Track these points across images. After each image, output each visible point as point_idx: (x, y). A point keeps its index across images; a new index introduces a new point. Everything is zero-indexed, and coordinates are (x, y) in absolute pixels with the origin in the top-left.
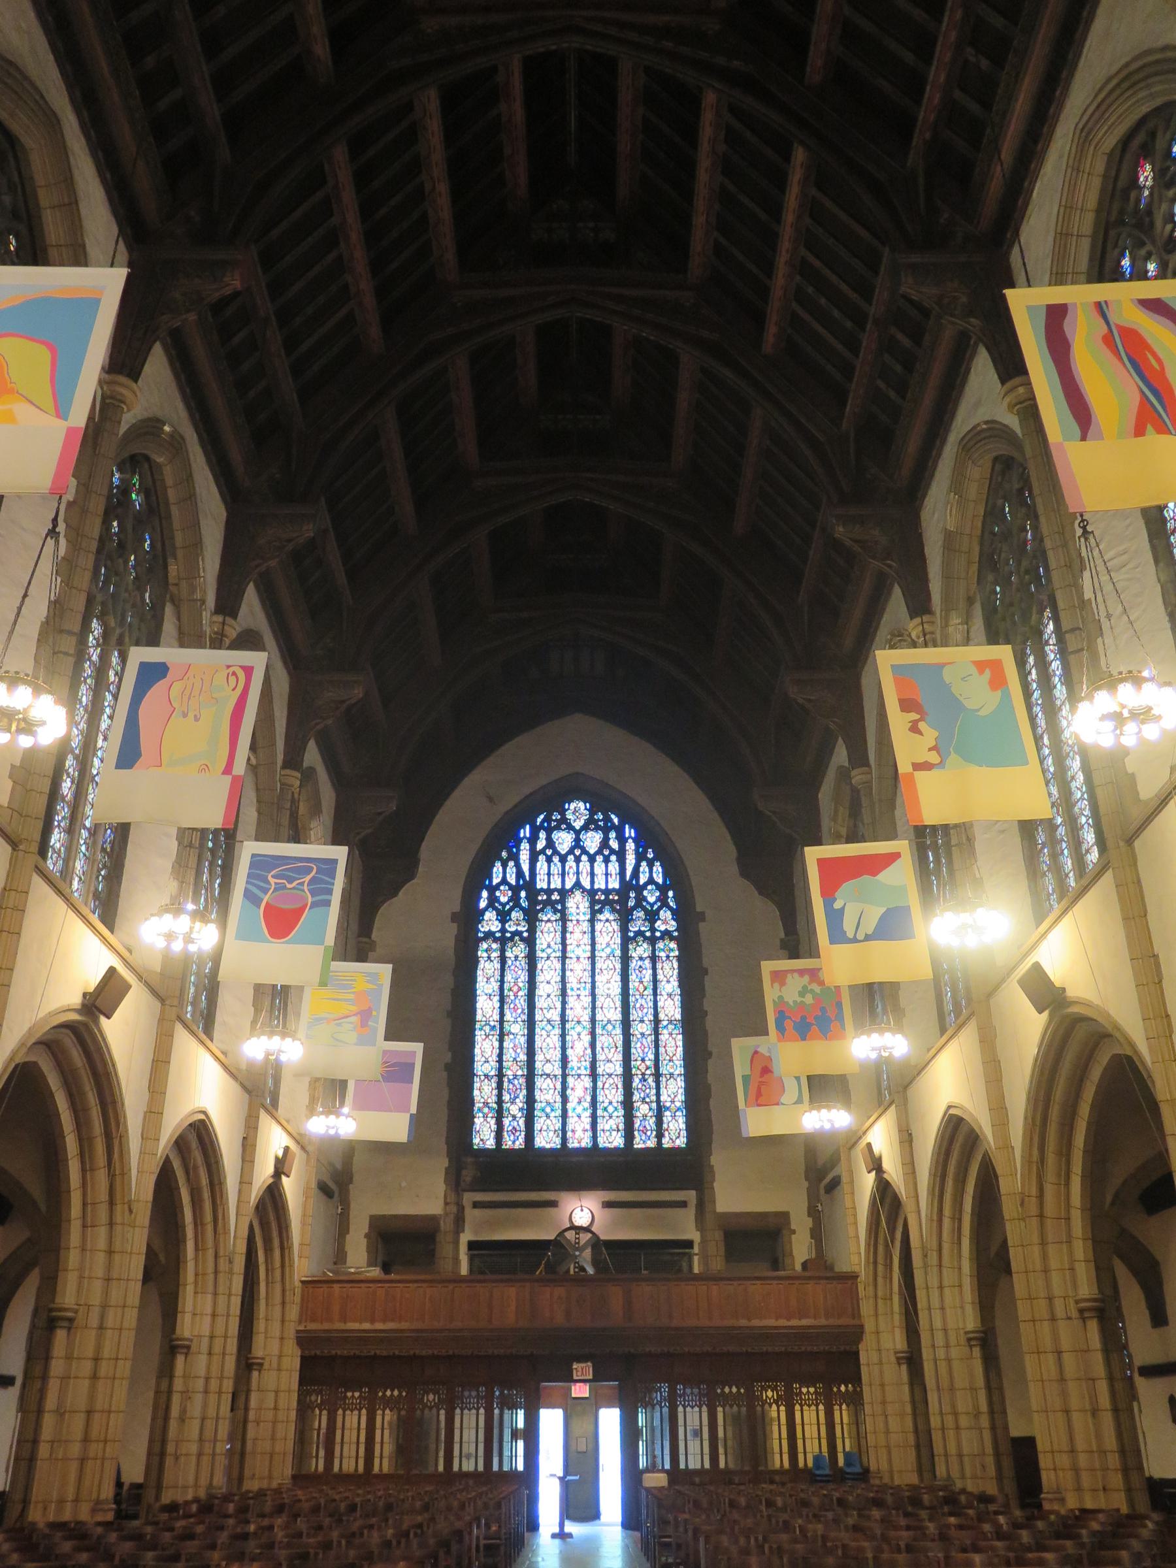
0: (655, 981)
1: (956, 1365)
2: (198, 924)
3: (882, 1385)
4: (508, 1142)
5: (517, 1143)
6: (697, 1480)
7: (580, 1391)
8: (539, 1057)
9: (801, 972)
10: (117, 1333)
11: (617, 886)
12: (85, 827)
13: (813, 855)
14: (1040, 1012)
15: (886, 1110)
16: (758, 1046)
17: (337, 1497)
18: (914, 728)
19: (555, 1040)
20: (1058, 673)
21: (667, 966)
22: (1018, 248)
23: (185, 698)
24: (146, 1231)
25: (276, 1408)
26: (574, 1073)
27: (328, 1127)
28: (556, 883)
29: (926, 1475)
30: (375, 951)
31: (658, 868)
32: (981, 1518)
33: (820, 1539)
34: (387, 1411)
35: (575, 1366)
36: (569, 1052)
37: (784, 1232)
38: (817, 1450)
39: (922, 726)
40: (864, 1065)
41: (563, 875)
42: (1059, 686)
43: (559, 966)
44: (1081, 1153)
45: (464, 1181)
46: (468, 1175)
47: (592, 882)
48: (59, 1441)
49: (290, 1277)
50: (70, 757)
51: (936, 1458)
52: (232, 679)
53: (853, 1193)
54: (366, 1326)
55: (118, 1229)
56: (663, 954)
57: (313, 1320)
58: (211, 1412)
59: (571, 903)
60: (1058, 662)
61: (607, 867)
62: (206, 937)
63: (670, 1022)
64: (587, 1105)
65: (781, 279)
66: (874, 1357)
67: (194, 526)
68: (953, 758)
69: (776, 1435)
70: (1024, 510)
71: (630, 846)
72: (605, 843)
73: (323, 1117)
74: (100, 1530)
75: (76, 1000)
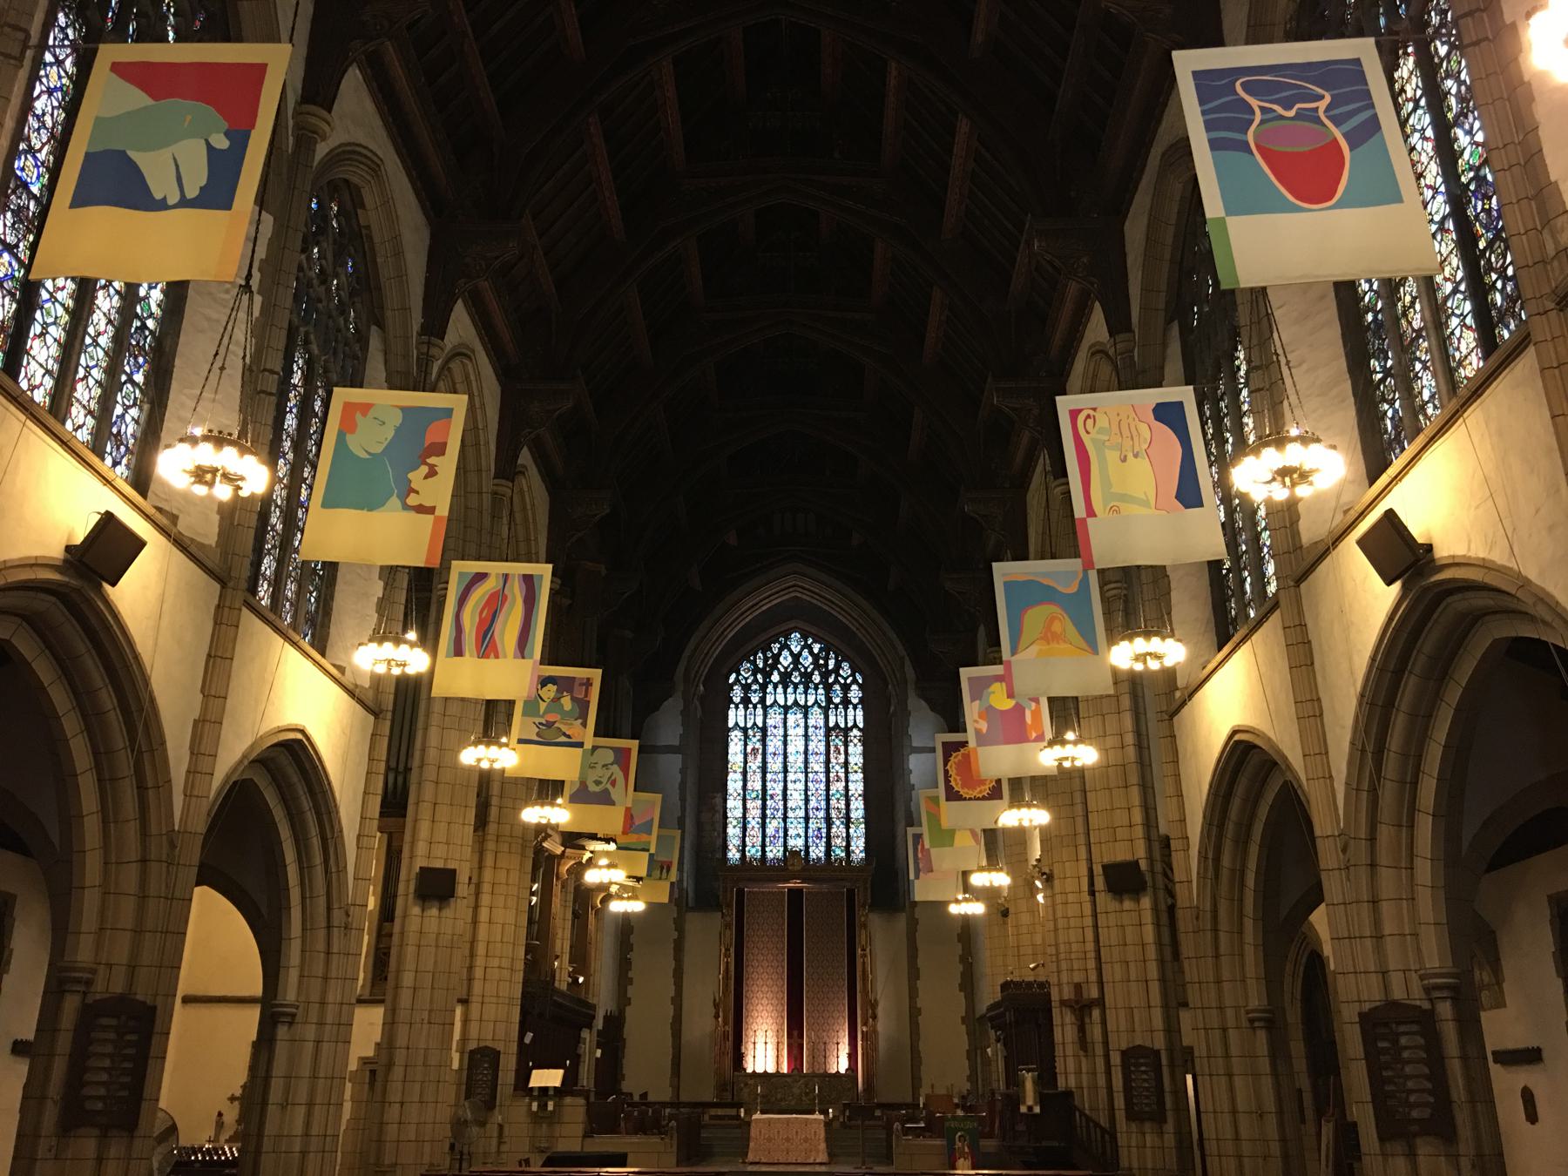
14: (1389, 584)
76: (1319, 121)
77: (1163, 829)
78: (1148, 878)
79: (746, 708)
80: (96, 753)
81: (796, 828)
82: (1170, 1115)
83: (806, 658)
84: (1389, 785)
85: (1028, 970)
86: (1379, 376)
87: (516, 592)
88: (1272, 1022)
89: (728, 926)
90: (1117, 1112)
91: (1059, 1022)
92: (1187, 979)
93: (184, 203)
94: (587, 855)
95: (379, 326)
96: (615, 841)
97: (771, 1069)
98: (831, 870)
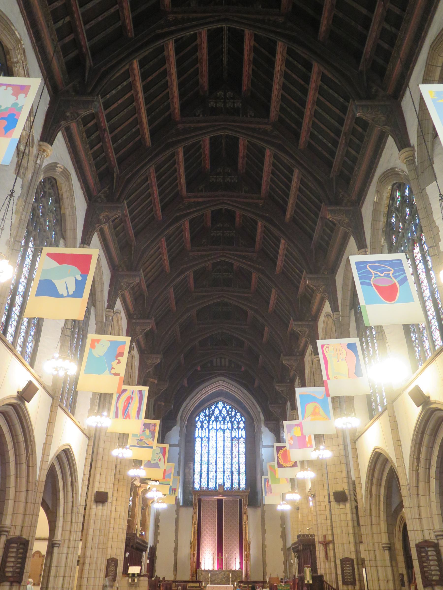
10: (73, 549)
12: (31, 335)
14: (418, 407)
44: (435, 468)
49: (76, 499)
65: (306, 123)
75: (15, 394)
76: (391, 278)
77: (353, 478)
78: (348, 496)
79: (202, 430)
80: (16, 455)
81: (220, 475)
82: (357, 583)
83: (224, 411)
84: (421, 468)
85: (306, 531)
86: (414, 339)
87: (136, 396)
88: (390, 548)
89: (195, 513)
90: (339, 582)
91: (318, 549)
92: (362, 533)
93: (69, 296)
94: (148, 486)
96: (158, 481)
97: (211, 568)
98: (231, 493)
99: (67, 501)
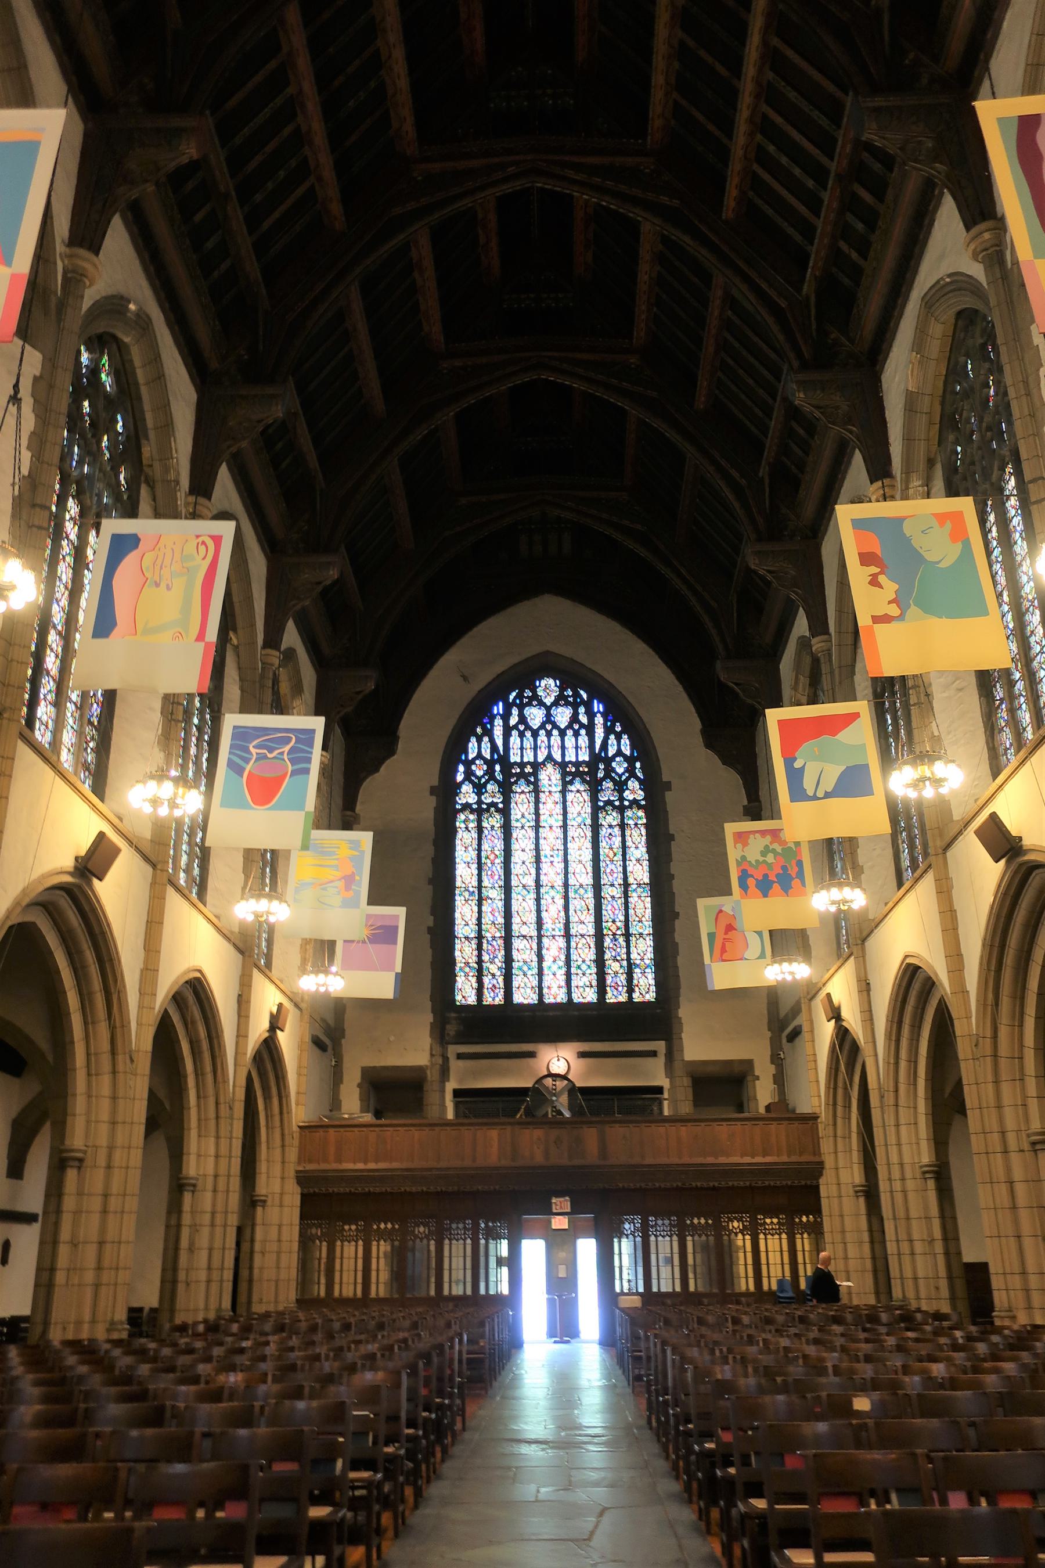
0: (624, 847)
1: (911, 1196)
2: (181, 790)
3: (842, 1216)
4: (488, 999)
5: (497, 999)
6: (669, 1302)
7: (560, 1223)
8: (516, 920)
9: (763, 833)
11: (587, 759)
13: (773, 716)
15: (846, 961)
16: (723, 905)
17: (334, 1318)
18: (874, 582)
19: (531, 904)
20: (1018, 529)
21: (635, 833)
22: (989, 82)
23: (158, 568)
24: (146, 1080)
25: (279, 1241)
26: (549, 934)
27: (317, 984)
28: (529, 757)
29: (883, 1297)
30: (359, 824)
31: (625, 740)
32: (937, 1333)
33: (781, 1349)
34: (382, 1242)
35: (554, 1200)
36: (544, 915)
37: (749, 1078)
38: (780, 1274)
39: (882, 579)
40: (823, 917)
41: (535, 748)
42: (1019, 542)
43: (533, 834)
45: (448, 1034)
46: (451, 1029)
47: (563, 755)
48: (75, 1269)
49: (289, 1122)
50: (52, 632)
51: (893, 1281)
52: (202, 549)
53: (813, 1041)
54: (360, 1166)
55: (121, 1077)
56: (631, 822)
57: (310, 1161)
58: (218, 1244)
59: (543, 775)
60: (1019, 518)
61: (577, 740)
62: (192, 802)
63: (639, 885)
64: (562, 964)
66: (834, 1189)
67: (164, 408)
68: (913, 610)
69: (742, 1261)
70: (987, 365)
71: (599, 720)
72: (574, 718)
73: (312, 976)
74: (107, 1346)
75: (69, 863)
95: (148, 484)
99: (92, 1017)
